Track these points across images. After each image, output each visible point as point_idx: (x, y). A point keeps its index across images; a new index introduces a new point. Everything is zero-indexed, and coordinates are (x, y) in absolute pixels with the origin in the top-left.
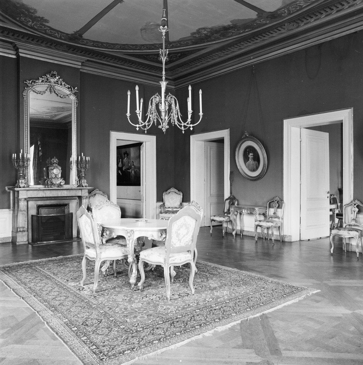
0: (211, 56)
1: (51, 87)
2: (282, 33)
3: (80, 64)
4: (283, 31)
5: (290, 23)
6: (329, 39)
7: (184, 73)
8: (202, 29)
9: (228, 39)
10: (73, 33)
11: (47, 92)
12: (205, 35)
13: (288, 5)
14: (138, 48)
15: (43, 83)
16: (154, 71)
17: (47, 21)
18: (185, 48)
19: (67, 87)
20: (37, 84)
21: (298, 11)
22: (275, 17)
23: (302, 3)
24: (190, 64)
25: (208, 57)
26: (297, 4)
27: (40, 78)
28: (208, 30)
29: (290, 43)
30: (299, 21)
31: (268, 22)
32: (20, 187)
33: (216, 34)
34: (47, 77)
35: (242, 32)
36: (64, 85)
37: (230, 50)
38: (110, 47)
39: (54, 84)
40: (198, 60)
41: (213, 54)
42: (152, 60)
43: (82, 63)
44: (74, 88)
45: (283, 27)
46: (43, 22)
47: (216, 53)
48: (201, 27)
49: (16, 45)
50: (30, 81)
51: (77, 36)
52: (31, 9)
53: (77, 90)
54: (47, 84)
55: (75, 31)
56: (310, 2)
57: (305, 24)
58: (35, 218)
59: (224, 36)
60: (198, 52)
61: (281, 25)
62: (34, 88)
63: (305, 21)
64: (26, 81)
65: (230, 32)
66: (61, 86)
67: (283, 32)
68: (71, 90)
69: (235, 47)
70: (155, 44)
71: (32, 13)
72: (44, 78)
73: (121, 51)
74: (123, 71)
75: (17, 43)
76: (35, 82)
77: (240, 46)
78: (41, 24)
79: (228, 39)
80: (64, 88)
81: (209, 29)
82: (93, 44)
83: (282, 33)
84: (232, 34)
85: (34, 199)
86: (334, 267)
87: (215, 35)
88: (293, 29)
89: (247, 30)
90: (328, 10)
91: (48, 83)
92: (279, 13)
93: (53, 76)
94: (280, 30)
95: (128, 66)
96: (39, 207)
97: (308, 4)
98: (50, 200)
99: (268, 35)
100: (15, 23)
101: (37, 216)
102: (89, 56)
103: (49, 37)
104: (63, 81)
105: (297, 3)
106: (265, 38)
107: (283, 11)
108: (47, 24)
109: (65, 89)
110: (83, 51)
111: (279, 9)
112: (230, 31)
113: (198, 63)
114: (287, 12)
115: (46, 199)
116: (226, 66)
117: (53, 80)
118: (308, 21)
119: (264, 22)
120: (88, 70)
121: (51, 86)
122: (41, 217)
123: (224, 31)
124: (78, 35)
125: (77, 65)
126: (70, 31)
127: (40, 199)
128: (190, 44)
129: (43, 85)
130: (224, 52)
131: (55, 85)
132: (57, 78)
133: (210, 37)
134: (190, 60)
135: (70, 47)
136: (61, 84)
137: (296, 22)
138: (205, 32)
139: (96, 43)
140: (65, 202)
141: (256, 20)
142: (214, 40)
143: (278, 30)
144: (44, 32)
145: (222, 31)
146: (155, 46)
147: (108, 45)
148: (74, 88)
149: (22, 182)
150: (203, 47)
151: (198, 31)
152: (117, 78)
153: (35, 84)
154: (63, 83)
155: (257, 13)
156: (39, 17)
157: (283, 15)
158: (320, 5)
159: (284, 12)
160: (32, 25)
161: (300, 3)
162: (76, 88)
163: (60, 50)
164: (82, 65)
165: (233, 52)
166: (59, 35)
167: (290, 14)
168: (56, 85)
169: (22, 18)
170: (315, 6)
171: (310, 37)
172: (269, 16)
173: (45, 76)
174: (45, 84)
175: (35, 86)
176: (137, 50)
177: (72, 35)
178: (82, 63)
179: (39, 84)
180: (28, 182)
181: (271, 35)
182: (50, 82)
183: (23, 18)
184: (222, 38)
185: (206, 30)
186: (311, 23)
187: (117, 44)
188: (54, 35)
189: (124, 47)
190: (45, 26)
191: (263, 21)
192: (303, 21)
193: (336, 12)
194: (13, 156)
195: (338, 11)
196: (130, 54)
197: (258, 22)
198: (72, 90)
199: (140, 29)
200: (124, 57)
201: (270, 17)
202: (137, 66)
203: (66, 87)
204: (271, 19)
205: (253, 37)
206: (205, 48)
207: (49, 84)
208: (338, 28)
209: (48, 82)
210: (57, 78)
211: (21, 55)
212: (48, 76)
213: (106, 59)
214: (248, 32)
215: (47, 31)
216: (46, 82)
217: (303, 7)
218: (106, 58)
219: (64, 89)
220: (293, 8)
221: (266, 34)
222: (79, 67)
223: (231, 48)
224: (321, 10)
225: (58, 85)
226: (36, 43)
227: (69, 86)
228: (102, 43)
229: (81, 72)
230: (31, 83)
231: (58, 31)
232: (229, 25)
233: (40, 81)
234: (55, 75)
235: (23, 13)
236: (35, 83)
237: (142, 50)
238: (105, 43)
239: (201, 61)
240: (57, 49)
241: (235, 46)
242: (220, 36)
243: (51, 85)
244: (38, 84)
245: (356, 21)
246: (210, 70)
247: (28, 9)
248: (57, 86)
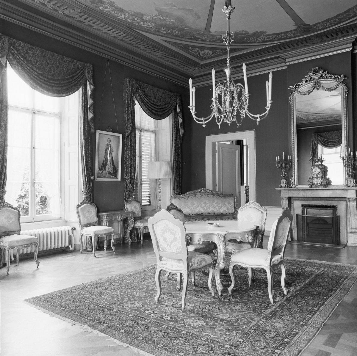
20: (302, 86)
27: (303, 79)
29: (158, 70)
32: (281, 187)
36: (330, 77)
58: (300, 218)
74: (204, 77)
80: (331, 80)
85: (300, 199)
86: (341, 257)
91: (312, 81)
96: (304, 206)
98: (316, 200)
100: (263, 45)
101: (302, 216)
115: (312, 199)
117: (316, 77)
122: (307, 217)
127: (305, 199)
132: (321, 72)
136: (326, 77)
140: (334, 203)
148: (340, 76)
149: (283, 182)
150: (245, 47)
154: (328, 75)
168: (321, 80)
180: (295, 182)
194: (276, 159)
203: (333, 79)
206: (247, 48)
210: (321, 72)
216: (310, 81)
225: (324, 79)
244: (303, 86)
248: (323, 80)
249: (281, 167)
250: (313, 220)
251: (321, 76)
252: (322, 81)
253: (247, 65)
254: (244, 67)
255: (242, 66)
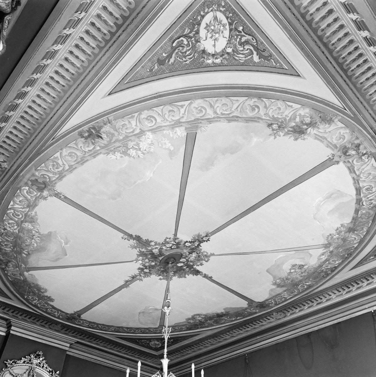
0: (204, 343)
1: (31, 370)
2: (271, 322)
3: (68, 345)
4: (272, 320)
5: (277, 312)
6: (316, 329)
7: (188, 356)
8: (197, 315)
9: (221, 326)
10: (73, 312)
11: (25, 375)
12: (199, 321)
13: (274, 296)
14: (132, 332)
15: (25, 364)
16: (143, 358)
17: (52, 300)
18: (178, 333)
19: (48, 370)
20: (18, 365)
21: (283, 302)
22: (264, 307)
23: (285, 295)
24: (182, 352)
25: (200, 344)
26: (282, 296)
28: (203, 316)
30: (285, 312)
31: (258, 311)
33: (210, 320)
34: (30, 357)
35: (234, 319)
36: (46, 368)
37: (223, 338)
38: (105, 329)
39: (35, 366)
40: (190, 347)
41: (206, 341)
42: (143, 345)
43: (71, 344)
44: (55, 373)
45: (272, 316)
46: (48, 301)
47: (209, 341)
48: (197, 313)
49: (11, 322)
50: (11, 361)
51: (75, 317)
52: (43, 289)
53: (58, 375)
54: (28, 366)
55: (76, 311)
56: (292, 295)
57: (291, 314)
59: (217, 322)
60: (191, 338)
61: (270, 314)
62: (12, 370)
63: (291, 312)
64: (7, 361)
65: (223, 319)
66: (42, 369)
67: (272, 321)
68: (52, 375)
69: (227, 334)
70: (150, 328)
71: (43, 293)
72: (27, 358)
73: (114, 333)
74: (111, 356)
75: (13, 320)
76: (15, 363)
77: (232, 334)
78: (45, 303)
79: (221, 326)
80: (45, 371)
81: (204, 315)
82: (88, 325)
83: (271, 322)
84: (225, 321)
87: (209, 321)
88: (281, 319)
89: (238, 318)
90: (309, 302)
91: (29, 365)
92: (267, 303)
93: (38, 356)
94: (269, 319)
95: (118, 351)
97: (292, 296)
99: (266, 321)
102: (81, 337)
103: (49, 316)
104: (46, 363)
105: (282, 295)
106: (256, 327)
107: (270, 301)
108: (51, 303)
109: (46, 373)
110: (75, 332)
111: (267, 300)
112: (223, 318)
113: (174, 356)
114: (274, 303)
116: (217, 355)
117: (35, 361)
118: (293, 311)
119: (254, 311)
120: (74, 353)
121: (32, 368)
123: (218, 318)
124: (77, 315)
125: (65, 346)
126: (70, 310)
128: (184, 330)
129: (23, 367)
130: (216, 339)
131: (36, 368)
132: (41, 359)
133: (204, 323)
134: (182, 347)
135: (64, 326)
136: (43, 367)
137: (283, 312)
138: (200, 318)
139: (92, 324)
141: (246, 309)
142: (208, 327)
143: (267, 319)
144: (45, 310)
145: (216, 318)
146: (150, 330)
147: (103, 327)
148: (55, 373)
150: (196, 333)
151: (193, 318)
152: (103, 364)
153: (15, 365)
154: (46, 366)
155: (247, 303)
156: (47, 296)
157: (270, 305)
158: (302, 297)
159: (271, 302)
160: (37, 303)
161: (285, 296)
162: (58, 372)
163: (53, 329)
164: (70, 347)
165: (226, 339)
166: (58, 314)
167: (276, 304)
168: (38, 367)
169: (30, 297)
170: (298, 298)
171: (298, 326)
172: (259, 306)
173: (29, 356)
174: (25, 366)
175: (14, 368)
176: (131, 333)
177: (72, 314)
178: (71, 344)
179: (20, 365)
181: (261, 324)
182: (32, 364)
183: (31, 296)
184: (215, 324)
185: (201, 316)
186: (296, 313)
187: (112, 326)
188: (54, 314)
189: (119, 329)
190: (48, 304)
191: (253, 310)
192: (289, 311)
193: (308, 308)
195: (318, 304)
196: (122, 338)
197: (248, 311)
198: (52, 374)
199: (139, 313)
200: (116, 340)
201: (259, 307)
202: (126, 351)
204: (260, 308)
205: (245, 325)
206: (199, 334)
207: (30, 366)
208: (340, 312)
209: (30, 364)
211: (12, 332)
212: (32, 356)
213: (97, 342)
214: (240, 320)
215: (48, 310)
216: (28, 363)
217: (287, 298)
218: (97, 340)
219: (45, 373)
220: (279, 299)
221: (257, 323)
222: (67, 349)
223: (224, 336)
224: (303, 302)
225: (40, 368)
226: (32, 321)
227: (51, 370)
228: (98, 324)
229: (67, 355)
230: (12, 363)
231: (58, 310)
232: (222, 313)
233: (22, 361)
234: (40, 355)
235: (33, 292)
236: (15, 364)
237: (136, 334)
238: (100, 324)
239: (193, 349)
240: (50, 328)
241: (228, 333)
242: (214, 322)
243: (32, 367)
244: (19, 366)
245: (336, 313)
246: (196, 361)
247: (39, 288)
248: (38, 369)
249: (12, 249)
250: (326, 4)
251: (40, 363)
252: (37, 369)
253: (142, 364)
254: (139, 364)
255: (137, 362)
